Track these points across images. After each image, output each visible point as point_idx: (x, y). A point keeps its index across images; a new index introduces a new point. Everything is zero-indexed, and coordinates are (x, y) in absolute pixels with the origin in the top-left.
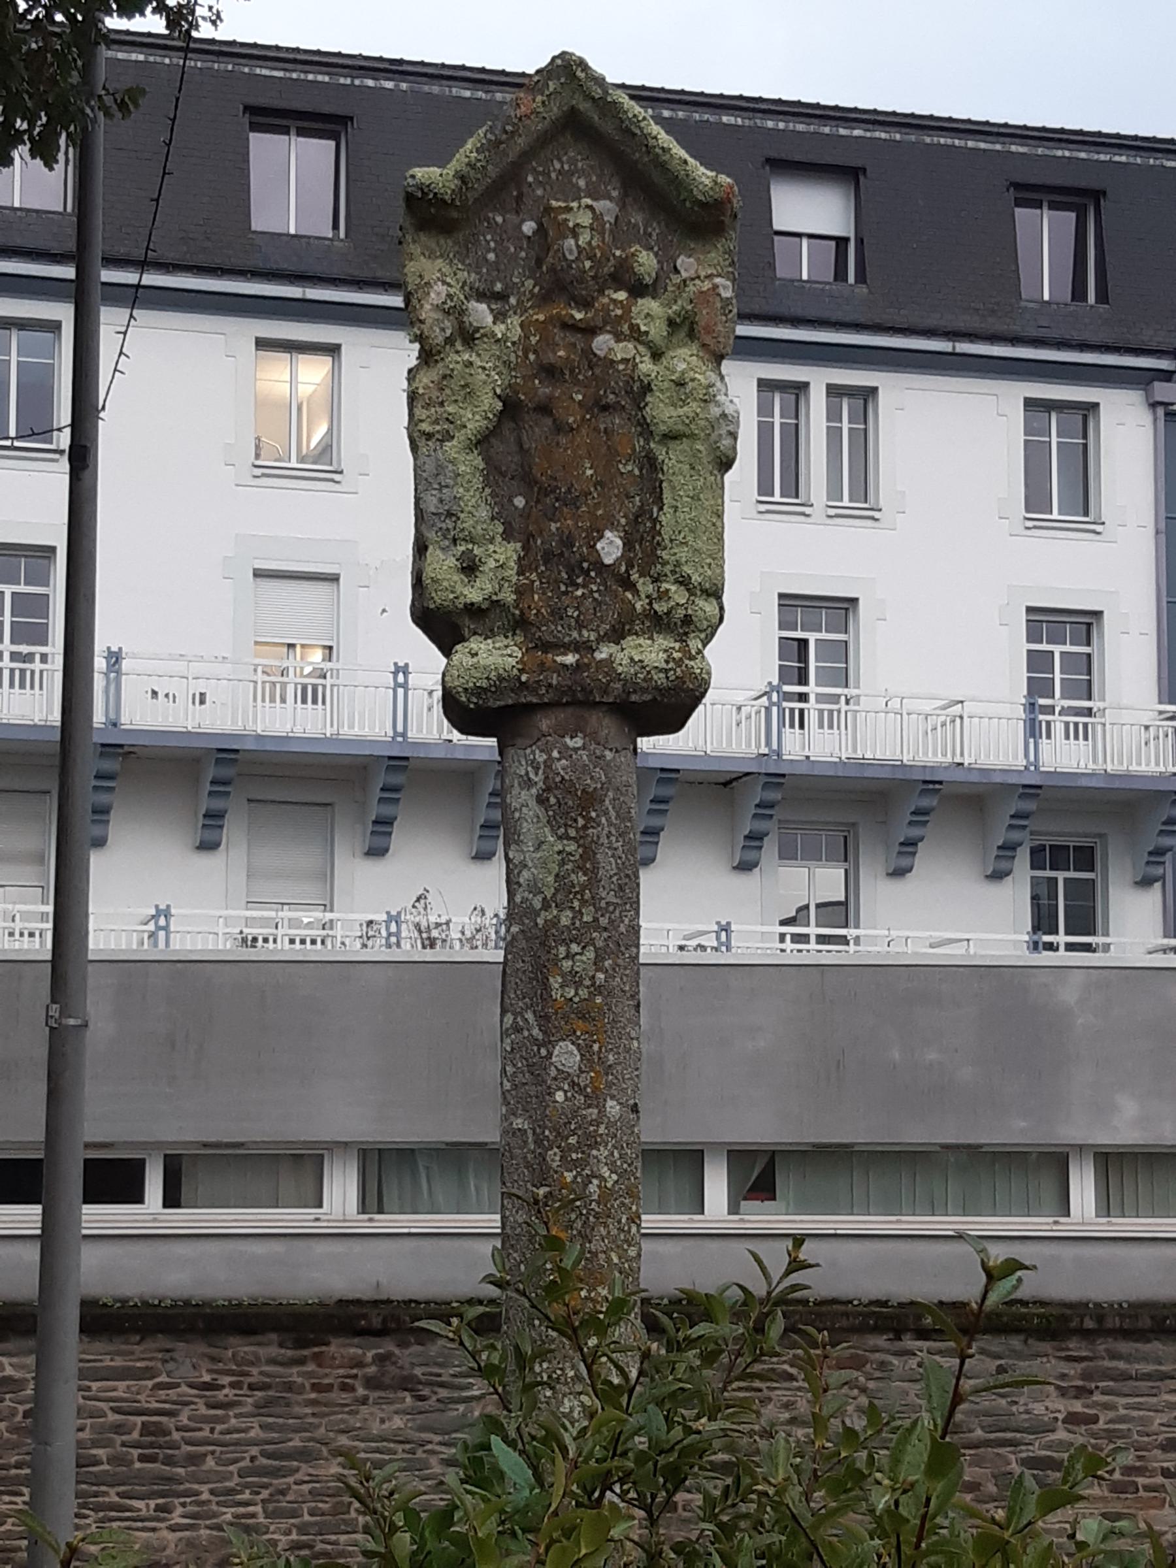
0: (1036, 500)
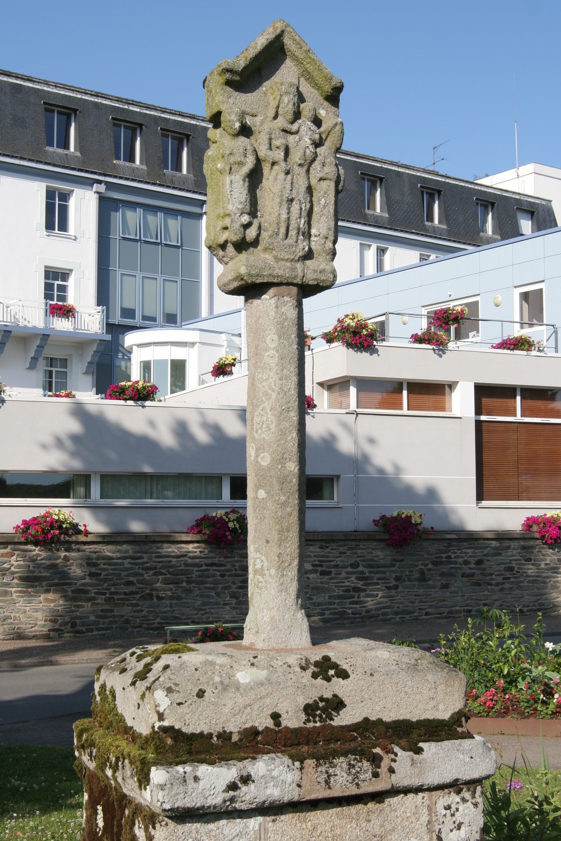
0: (49, 226)
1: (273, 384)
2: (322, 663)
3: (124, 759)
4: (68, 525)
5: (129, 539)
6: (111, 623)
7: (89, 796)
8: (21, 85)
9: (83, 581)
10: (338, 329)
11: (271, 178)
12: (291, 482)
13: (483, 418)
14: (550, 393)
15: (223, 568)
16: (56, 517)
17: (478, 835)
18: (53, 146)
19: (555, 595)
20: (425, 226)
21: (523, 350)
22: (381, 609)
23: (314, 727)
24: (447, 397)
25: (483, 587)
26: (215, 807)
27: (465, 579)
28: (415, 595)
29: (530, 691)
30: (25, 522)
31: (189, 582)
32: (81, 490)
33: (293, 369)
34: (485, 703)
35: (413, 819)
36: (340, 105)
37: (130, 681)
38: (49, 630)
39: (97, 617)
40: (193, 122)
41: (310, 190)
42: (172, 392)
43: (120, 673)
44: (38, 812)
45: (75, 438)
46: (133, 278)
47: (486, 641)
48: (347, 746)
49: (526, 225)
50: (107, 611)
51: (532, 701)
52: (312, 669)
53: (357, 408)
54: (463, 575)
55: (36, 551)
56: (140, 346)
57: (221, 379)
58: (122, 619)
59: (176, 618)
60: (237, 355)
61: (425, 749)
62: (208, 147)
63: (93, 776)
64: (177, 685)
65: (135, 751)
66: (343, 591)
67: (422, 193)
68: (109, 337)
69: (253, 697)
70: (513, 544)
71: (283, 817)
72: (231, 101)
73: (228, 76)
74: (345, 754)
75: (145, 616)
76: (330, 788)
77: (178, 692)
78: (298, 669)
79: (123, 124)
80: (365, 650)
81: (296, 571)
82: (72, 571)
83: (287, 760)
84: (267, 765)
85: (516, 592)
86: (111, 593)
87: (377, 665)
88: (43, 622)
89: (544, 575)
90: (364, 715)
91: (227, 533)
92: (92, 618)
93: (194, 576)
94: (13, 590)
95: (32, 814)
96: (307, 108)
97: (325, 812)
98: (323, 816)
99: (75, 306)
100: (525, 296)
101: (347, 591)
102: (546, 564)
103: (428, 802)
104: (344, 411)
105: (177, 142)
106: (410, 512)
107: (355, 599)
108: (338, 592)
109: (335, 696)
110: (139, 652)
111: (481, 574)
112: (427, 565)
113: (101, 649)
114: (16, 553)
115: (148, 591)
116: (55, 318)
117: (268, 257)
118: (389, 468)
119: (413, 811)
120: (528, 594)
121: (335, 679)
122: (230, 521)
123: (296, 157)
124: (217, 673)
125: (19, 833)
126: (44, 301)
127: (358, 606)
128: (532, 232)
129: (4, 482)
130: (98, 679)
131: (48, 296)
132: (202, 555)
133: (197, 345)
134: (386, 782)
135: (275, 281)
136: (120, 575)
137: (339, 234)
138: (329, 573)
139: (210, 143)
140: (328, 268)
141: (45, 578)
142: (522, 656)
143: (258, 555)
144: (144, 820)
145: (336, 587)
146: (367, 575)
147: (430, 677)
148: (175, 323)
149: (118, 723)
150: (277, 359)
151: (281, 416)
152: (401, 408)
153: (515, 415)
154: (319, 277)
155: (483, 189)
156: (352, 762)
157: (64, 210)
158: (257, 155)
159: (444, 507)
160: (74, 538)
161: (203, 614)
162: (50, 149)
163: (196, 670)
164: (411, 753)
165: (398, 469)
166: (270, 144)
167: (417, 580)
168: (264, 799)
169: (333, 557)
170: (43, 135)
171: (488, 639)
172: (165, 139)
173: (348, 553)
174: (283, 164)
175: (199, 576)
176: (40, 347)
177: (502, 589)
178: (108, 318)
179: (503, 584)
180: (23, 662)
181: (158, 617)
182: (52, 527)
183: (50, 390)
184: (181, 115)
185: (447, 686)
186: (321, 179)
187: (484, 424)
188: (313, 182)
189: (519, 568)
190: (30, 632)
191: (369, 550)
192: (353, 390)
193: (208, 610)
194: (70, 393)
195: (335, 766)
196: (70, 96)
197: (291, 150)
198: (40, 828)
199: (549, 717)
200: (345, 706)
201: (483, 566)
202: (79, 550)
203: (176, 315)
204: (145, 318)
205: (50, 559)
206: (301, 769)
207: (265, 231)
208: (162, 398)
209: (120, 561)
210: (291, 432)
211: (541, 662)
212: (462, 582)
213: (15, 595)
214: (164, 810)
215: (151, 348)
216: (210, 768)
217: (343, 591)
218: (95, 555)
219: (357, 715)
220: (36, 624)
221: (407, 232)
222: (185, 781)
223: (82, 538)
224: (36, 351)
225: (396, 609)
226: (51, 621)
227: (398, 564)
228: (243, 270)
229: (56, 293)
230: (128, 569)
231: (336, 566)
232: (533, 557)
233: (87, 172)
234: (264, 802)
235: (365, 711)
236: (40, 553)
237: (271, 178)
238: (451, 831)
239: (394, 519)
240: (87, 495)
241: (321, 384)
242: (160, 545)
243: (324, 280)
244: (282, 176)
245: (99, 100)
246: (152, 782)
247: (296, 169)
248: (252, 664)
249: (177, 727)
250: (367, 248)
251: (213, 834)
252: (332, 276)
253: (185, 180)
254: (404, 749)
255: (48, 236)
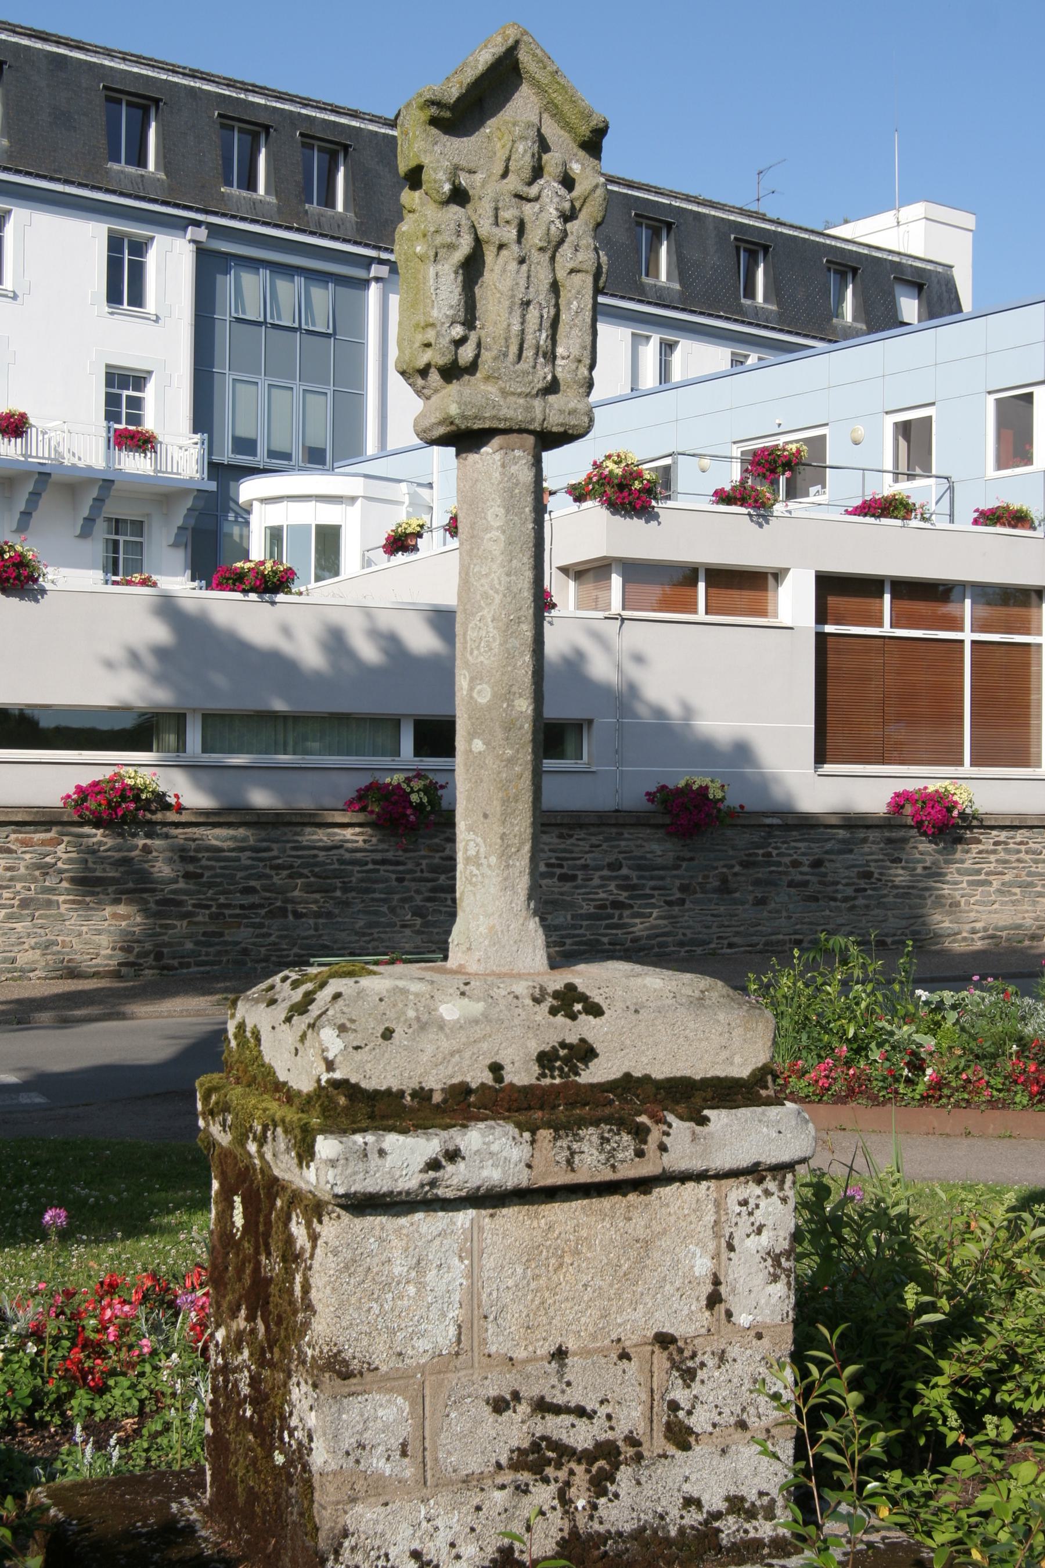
0: (114, 297)
1: (496, 582)
2: (564, 994)
3: (275, 1126)
4: (149, 795)
5: (248, 818)
6: (219, 953)
7: (221, 1185)
8: (66, 56)
9: (174, 886)
10: (595, 479)
11: (497, 269)
12: (521, 728)
13: (829, 629)
14: (941, 588)
15: (401, 868)
16: (131, 782)
17: (787, 1242)
18: (119, 161)
19: (937, 917)
20: (740, 305)
21: (896, 518)
22: (657, 936)
23: (552, 1085)
24: (770, 594)
25: (821, 903)
26: (408, 1193)
27: (793, 890)
28: (713, 915)
29: (887, 1064)
30: (79, 789)
31: (345, 890)
32: (172, 739)
33: (527, 559)
34: (817, 1081)
35: (693, 1218)
36: (604, 155)
37: (283, 1017)
38: (119, 964)
39: (197, 943)
40: (355, 123)
41: (555, 287)
42: (318, 579)
43: (268, 1006)
44: (119, 1234)
45: (161, 653)
46: (253, 388)
47: (823, 984)
48: (599, 1112)
49: (909, 307)
50: (214, 934)
51: (890, 1079)
52: (550, 1001)
53: (624, 609)
54: (791, 884)
55: (97, 835)
56: (264, 501)
57: (400, 558)
58: (238, 948)
59: (325, 947)
60: (425, 519)
61: (712, 1118)
62: (401, 219)
63: (226, 1154)
64: (353, 1021)
65: (291, 1115)
66: (596, 907)
67: (738, 249)
68: (212, 486)
69: (464, 1040)
70: (873, 835)
71: (505, 1211)
72: (438, 149)
73: (434, 111)
74: (596, 1123)
75: (275, 944)
76: (573, 1170)
77: (355, 1031)
78: (529, 1002)
79: (237, 124)
80: (628, 977)
81: (528, 861)
82: (156, 869)
83: (511, 1129)
84: (483, 1136)
85: (876, 912)
86: (221, 906)
87: (644, 999)
88: (109, 951)
89: (921, 885)
90: (625, 1070)
91: (409, 812)
92: (189, 945)
93: (354, 879)
94: (61, 898)
95: (112, 1240)
96: (552, 161)
97: (566, 1205)
98: (562, 1210)
99: (156, 432)
100: (905, 429)
101: (603, 907)
102: (925, 868)
103: (715, 1195)
104: (601, 615)
105: (327, 157)
106: (706, 781)
107: (615, 921)
108: (587, 908)
109: (583, 1041)
110: (294, 976)
111: (820, 883)
112: (732, 867)
113: (204, 994)
114: (66, 839)
115: (279, 904)
116: (124, 453)
117: (492, 390)
118: (674, 708)
119: (694, 1206)
120: (894, 916)
121: (583, 1017)
122: (412, 791)
123: (535, 236)
124: (411, 1005)
125: (91, 1263)
126: (104, 423)
127: (619, 932)
128: (920, 321)
129: (37, 723)
130: (233, 1016)
131: (112, 416)
132: (366, 846)
133: (360, 500)
134: (654, 1163)
135: (501, 426)
136: (233, 877)
137: (599, 317)
138: (574, 878)
139: (405, 212)
140: (581, 407)
141: (113, 881)
142: (878, 1010)
143: (472, 836)
144: (305, 1213)
145: (584, 900)
146: (635, 881)
147: (721, 1016)
148: (323, 462)
149: (264, 1077)
150: (502, 545)
151: (508, 629)
152: (695, 611)
153: (880, 625)
154: (567, 420)
155: (839, 245)
156: (606, 1135)
157: (138, 272)
158: (476, 234)
159: (762, 774)
160: (159, 817)
161: (369, 942)
162: (115, 166)
163: (381, 1000)
164: (692, 1124)
165: (689, 711)
166: (496, 217)
167: (716, 891)
168: (478, 1183)
169: (581, 852)
170: (103, 142)
171: (824, 984)
172: (307, 151)
173: (605, 846)
174: (515, 248)
175: (362, 880)
176: (99, 501)
177: (852, 908)
178: (210, 453)
179: (855, 898)
180: (78, 1013)
181: (294, 945)
182: (124, 798)
183: (115, 573)
184: (335, 110)
185: (747, 1030)
186: (572, 271)
187: (829, 639)
188: (561, 275)
189: (881, 874)
190: (88, 966)
191: (639, 842)
192: (616, 581)
193: (376, 936)
194: (149, 579)
195: (581, 1140)
196: (147, 76)
197: (528, 226)
198: (124, 1256)
199: (916, 1103)
200: (596, 1055)
201: (823, 870)
202: (167, 836)
203: (324, 451)
204: (272, 454)
205: (120, 850)
206: (533, 1142)
207: (486, 349)
208: (303, 589)
209: (233, 854)
210: (522, 654)
211: (908, 1018)
212: (789, 895)
213: (63, 908)
214: (336, 1196)
215: (284, 505)
216: (401, 1138)
217: (596, 907)
218: (193, 845)
219: (615, 1068)
220: (98, 955)
221: (710, 315)
222: (366, 1155)
223: (172, 816)
224: (92, 508)
225: (680, 937)
226: (121, 949)
227: (684, 864)
228: (454, 410)
229: (124, 410)
230: (247, 868)
231: (585, 867)
232: (904, 857)
233: (177, 206)
234: (479, 1188)
235: (627, 1063)
236: (105, 839)
237: (497, 269)
238: (748, 1236)
239: (679, 792)
240: (181, 747)
241: (564, 570)
242: (298, 829)
243: (574, 426)
244: (513, 266)
245: (197, 84)
246: (318, 1156)
247: (535, 256)
248: (463, 994)
249: (353, 1081)
250: (644, 341)
251: (404, 1231)
252: (586, 420)
253: (340, 222)
254: (681, 1118)
255: (112, 313)
